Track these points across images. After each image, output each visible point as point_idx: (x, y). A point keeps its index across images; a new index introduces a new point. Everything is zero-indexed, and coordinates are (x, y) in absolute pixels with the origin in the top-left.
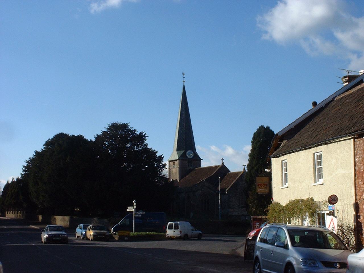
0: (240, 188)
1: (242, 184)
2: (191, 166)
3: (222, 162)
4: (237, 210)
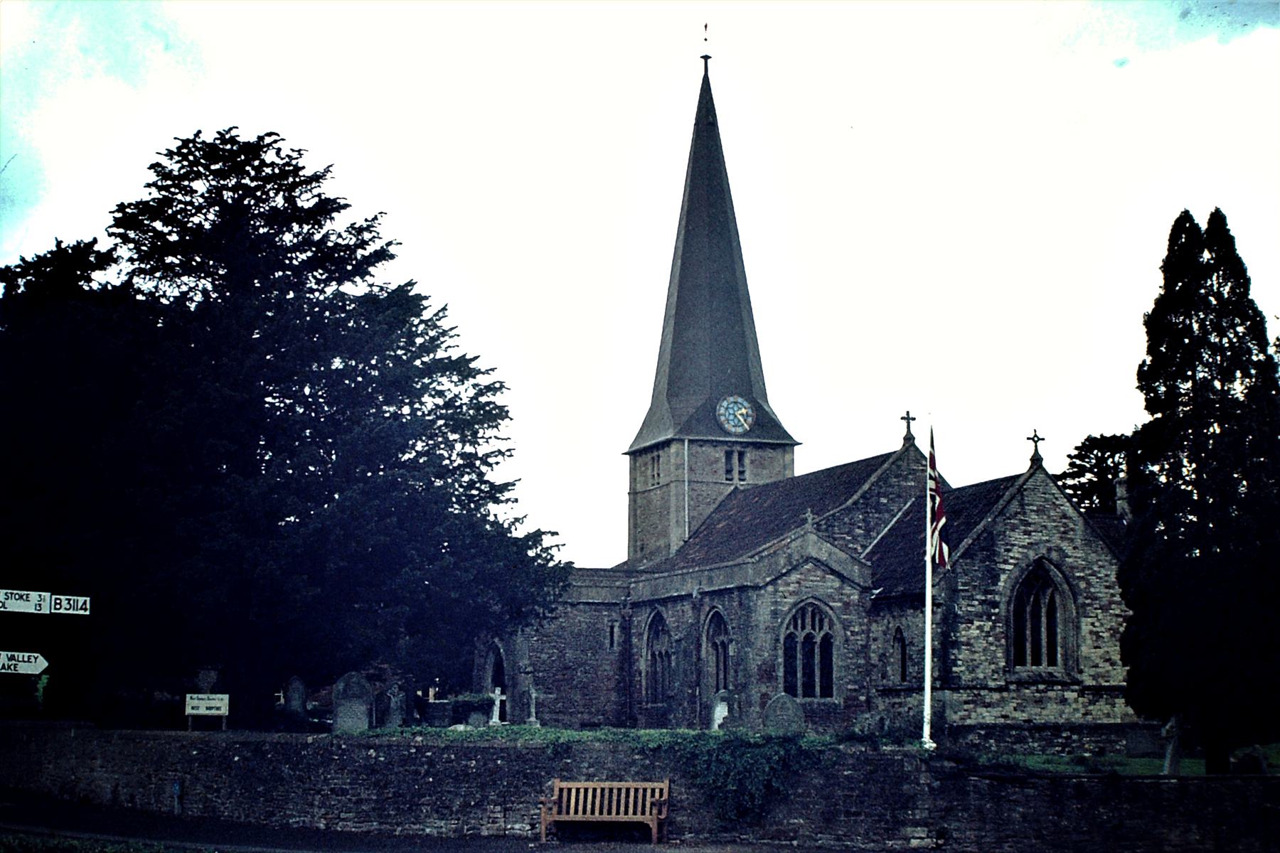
0: (1010, 567)
1: (1023, 547)
2: (741, 473)
3: (904, 432)
4: (996, 696)
